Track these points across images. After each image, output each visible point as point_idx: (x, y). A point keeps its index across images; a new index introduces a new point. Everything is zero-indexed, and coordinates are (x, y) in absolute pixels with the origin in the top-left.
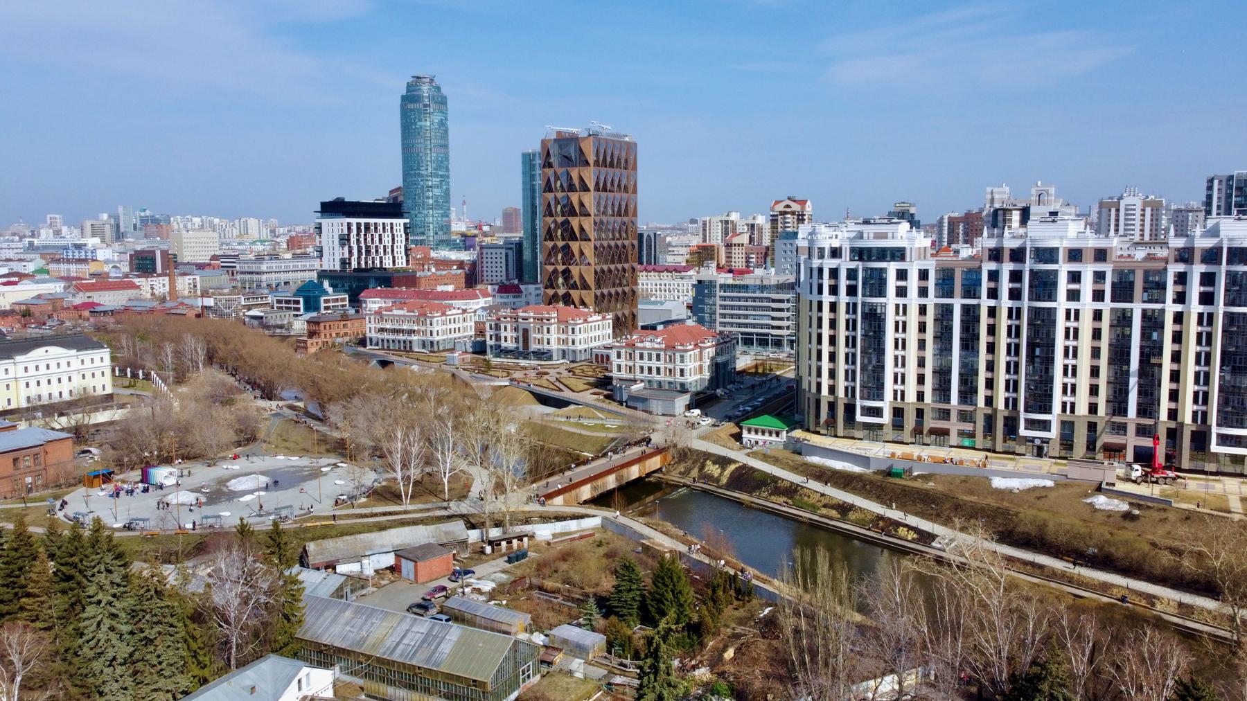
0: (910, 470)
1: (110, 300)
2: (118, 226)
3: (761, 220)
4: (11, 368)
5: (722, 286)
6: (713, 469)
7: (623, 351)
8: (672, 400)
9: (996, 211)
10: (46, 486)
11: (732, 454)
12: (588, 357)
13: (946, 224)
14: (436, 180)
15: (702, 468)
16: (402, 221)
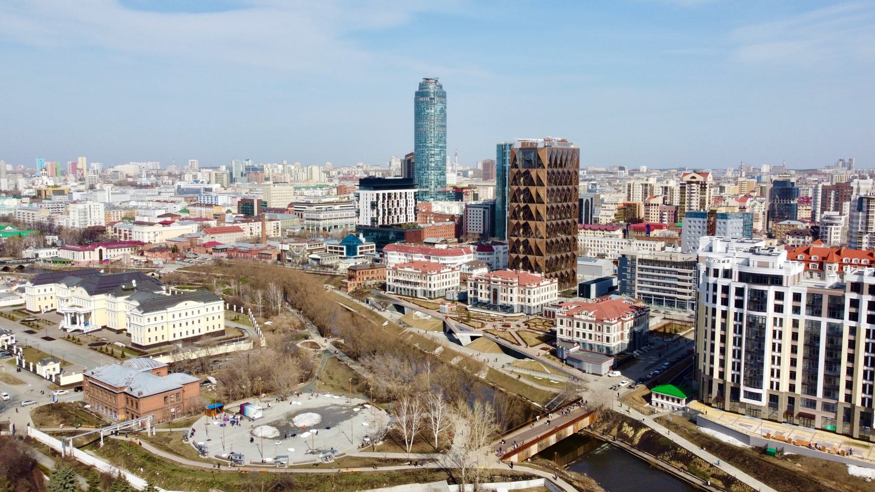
0: (782, 451)
1: (227, 240)
2: (231, 174)
3: (673, 184)
4: (165, 315)
5: (640, 260)
6: (628, 430)
7: (565, 320)
8: (600, 362)
9: (861, 199)
10: (183, 414)
12: (540, 310)
13: (820, 191)
14: (437, 150)
15: (620, 429)
16: (412, 191)
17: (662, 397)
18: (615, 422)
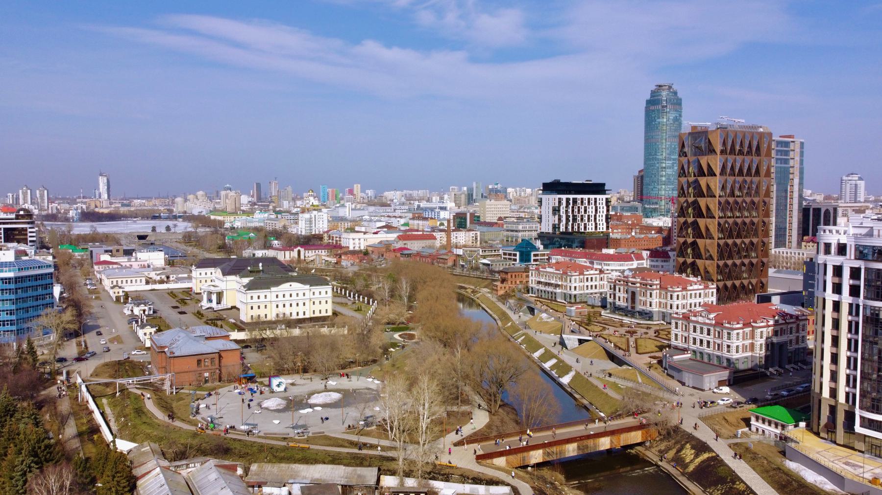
4: (268, 295)
7: (680, 322)
11: (712, 443)
15: (679, 451)
16: (604, 197)
17: (764, 421)
18: (676, 443)
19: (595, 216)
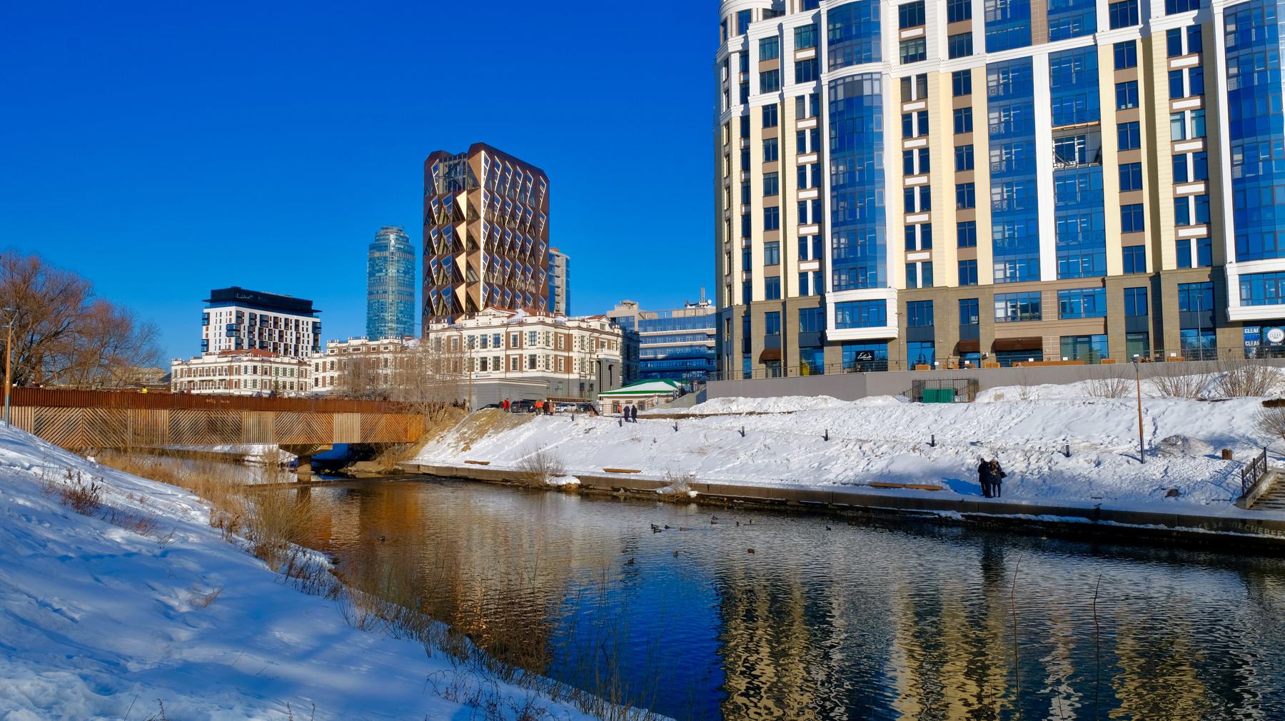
16: (311, 320)
19: (296, 347)
